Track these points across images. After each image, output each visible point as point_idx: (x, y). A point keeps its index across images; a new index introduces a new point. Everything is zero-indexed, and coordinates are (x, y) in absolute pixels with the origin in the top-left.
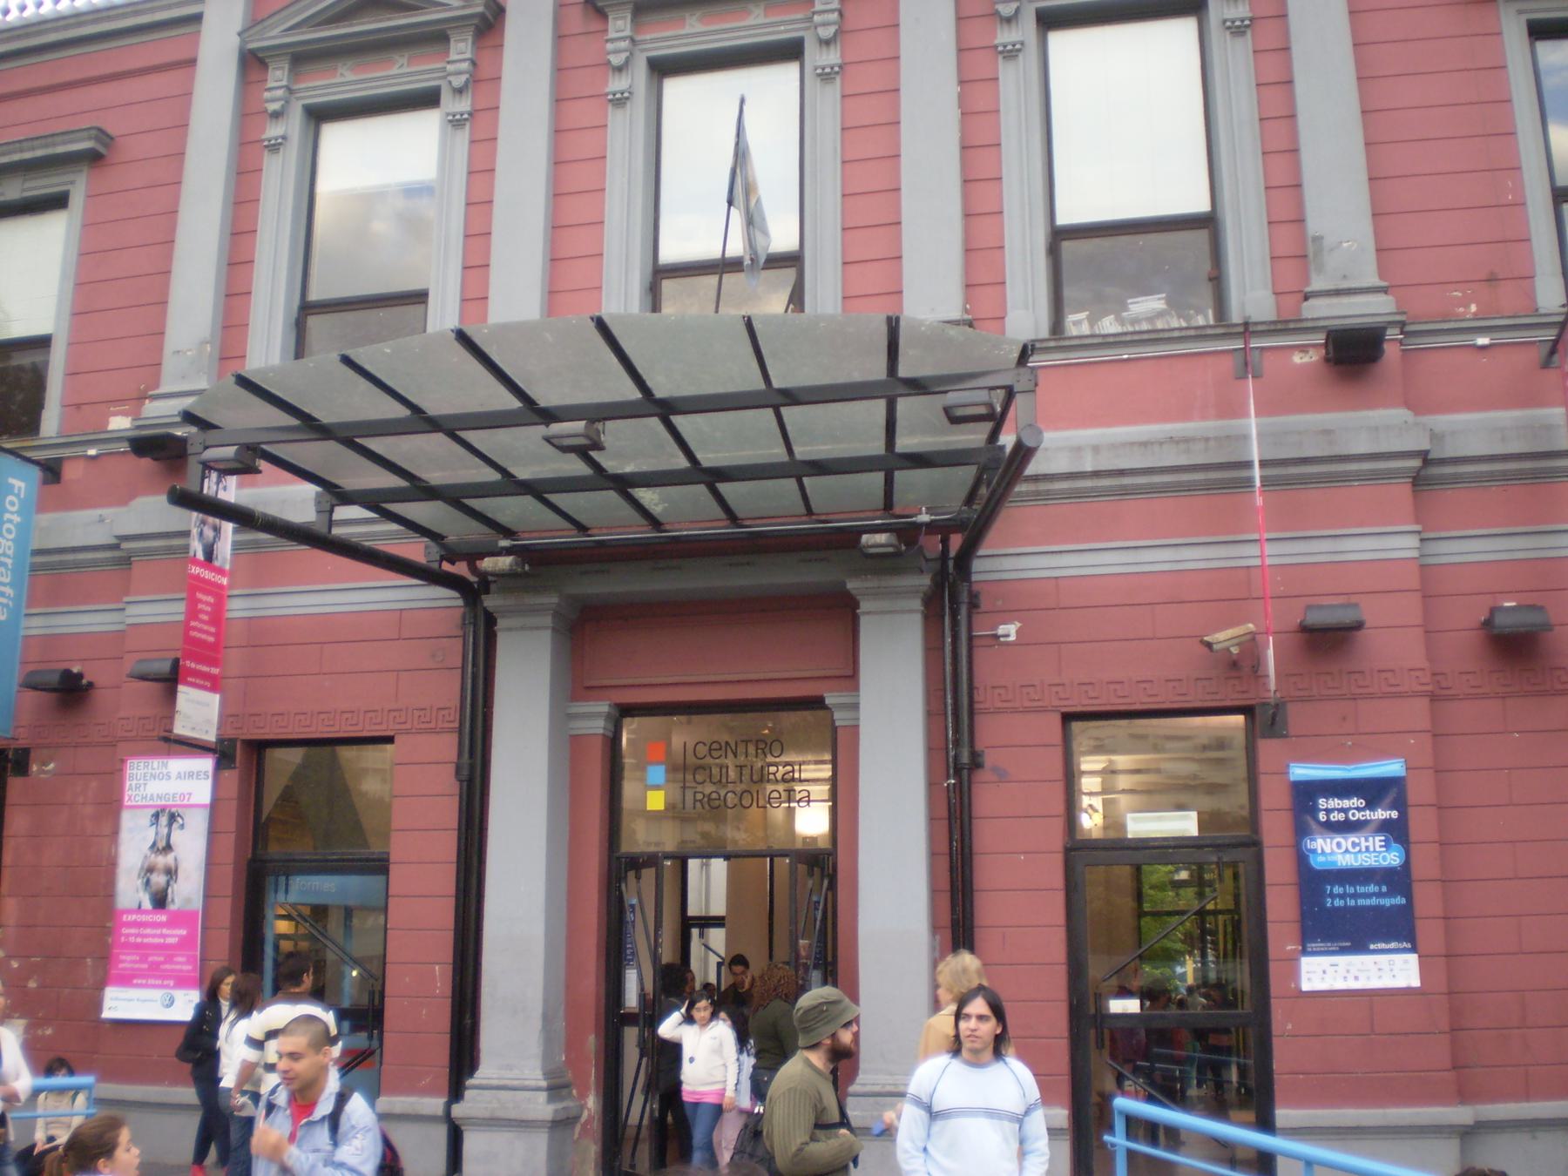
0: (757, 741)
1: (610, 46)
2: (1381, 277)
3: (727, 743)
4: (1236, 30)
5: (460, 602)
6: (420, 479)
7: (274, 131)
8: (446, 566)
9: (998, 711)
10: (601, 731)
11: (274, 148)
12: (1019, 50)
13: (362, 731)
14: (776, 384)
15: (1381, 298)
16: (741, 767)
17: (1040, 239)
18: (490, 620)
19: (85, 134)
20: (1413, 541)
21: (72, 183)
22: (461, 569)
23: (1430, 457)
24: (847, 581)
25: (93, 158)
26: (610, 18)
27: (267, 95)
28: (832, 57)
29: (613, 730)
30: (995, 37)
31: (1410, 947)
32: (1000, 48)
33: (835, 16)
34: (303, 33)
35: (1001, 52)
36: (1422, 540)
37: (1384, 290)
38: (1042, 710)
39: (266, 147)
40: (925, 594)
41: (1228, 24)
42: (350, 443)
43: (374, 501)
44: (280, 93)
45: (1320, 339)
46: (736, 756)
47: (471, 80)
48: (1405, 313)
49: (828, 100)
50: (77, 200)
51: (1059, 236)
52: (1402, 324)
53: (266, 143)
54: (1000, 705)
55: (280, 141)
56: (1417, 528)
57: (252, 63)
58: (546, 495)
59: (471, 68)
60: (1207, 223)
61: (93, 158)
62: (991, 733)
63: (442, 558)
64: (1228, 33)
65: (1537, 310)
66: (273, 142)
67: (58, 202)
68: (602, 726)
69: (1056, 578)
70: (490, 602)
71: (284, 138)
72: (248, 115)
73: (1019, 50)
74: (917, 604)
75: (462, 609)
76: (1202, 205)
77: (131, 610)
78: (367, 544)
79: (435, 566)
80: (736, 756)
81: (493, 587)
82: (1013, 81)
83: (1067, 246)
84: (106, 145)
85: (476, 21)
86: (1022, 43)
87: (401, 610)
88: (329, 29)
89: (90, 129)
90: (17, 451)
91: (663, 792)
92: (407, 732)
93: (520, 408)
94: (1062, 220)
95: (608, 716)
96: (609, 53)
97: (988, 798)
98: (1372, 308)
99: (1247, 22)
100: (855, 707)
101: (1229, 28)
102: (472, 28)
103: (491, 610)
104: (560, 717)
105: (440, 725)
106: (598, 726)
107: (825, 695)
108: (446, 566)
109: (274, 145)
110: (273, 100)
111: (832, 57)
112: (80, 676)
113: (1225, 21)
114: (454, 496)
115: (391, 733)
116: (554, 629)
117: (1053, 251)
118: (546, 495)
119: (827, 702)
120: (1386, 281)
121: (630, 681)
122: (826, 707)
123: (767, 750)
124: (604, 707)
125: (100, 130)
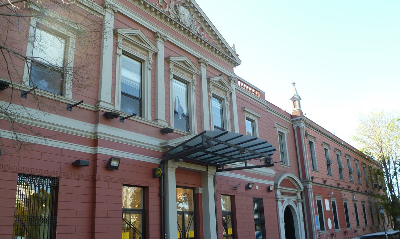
91: (329, 210)
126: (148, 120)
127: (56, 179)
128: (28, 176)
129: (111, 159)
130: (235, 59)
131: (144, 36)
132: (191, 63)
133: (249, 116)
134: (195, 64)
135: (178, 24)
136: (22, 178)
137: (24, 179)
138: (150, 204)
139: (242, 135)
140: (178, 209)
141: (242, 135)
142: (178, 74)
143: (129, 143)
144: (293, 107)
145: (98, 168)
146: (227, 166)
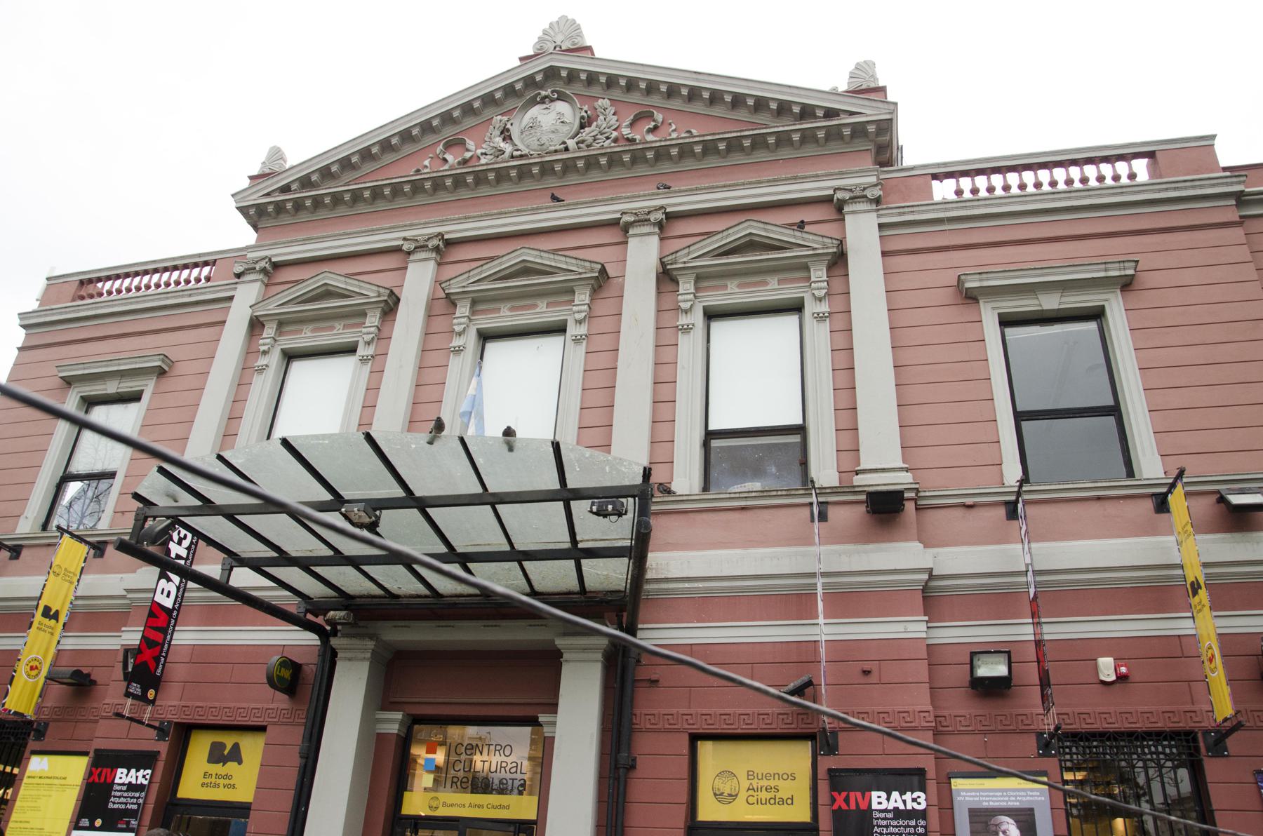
0: (496, 745)
1: (455, 321)
2: (904, 462)
3: (477, 745)
4: (820, 318)
5: (319, 643)
6: (285, 553)
7: (262, 361)
8: (309, 617)
9: (648, 731)
10: (396, 732)
11: (261, 371)
12: (691, 329)
13: (234, 721)
14: (490, 490)
15: (904, 474)
16: (484, 761)
17: (698, 436)
18: (334, 654)
19: (158, 357)
20: (923, 627)
21: (147, 385)
22: (320, 620)
23: (934, 574)
24: (555, 639)
25: (161, 372)
26: (458, 306)
27: (261, 342)
28: (583, 330)
29: (406, 732)
30: (678, 321)
31: (477, 758)
32: (680, 327)
33: (586, 307)
34: (289, 308)
35: (681, 330)
36: (928, 628)
37: (907, 470)
38: (677, 731)
39: (256, 370)
40: (605, 650)
41: (816, 315)
42: (231, 517)
43: (257, 565)
44: (268, 341)
45: (863, 497)
46: (481, 754)
47: (376, 338)
48: (918, 483)
49: (578, 354)
50: (146, 397)
51: (710, 435)
52: (917, 490)
53: (256, 368)
54: (649, 726)
55: (264, 367)
56: (926, 618)
57: (256, 325)
58: (361, 567)
59: (377, 331)
60: (801, 430)
61: (161, 372)
62: (644, 745)
63: (307, 611)
64: (815, 320)
65: (1003, 484)
66: (260, 368)
67: (135, 397)
68: (397, 728)
69: (691, 644)
70: (334, 642)
71: (267, 366)
72: (250, 351)
73: (691, 329)
74: (599, 656)
75: (319, 647)
76: (800, 422)
77: (125, 635)
78: (273, 603)
79: (302, 615)
80: (481, 754)
81: (339, 634)
82: (688, 348)
83: (715, 443)
84: (170, 367)
85: (382, 305)
86: (693, 325)
87: (284, 645)
88: (304, 306)
89: (159, 355)
90: (82, 537)
92: (275, 724)
93: (332, 500)
94: (711, 428)
95: (402, 723)
96: (455, 325)
97: (639, 789)
98: (902, 480)
99: (826, 314)
100: (554, 724)
101: (815, 318)
102: (380, 309)
103: (334, 646)
104: (368, 720)
105: (296, 720)
106: (394, 728)
107: (539, 715)
108: (309, 617)
109: (260, 370)
110: (264, 345)
111: (583, 330)
112: (88, 675)
113: (813, 314)
114: (306, 564)
115: (265, 724)
116: (371, 662)
117: (706, 445)
118: (361, 567)
119: (540, 719)
120: (906, 464)
121: (417, 700)
122: (540, 725)
123: (502, 752)
124: (399, 716)
125: (165, 356)
126: (1006, 484)
127: (1183, 737)
128: (1114, 737)
129: (976, 653)
130: (852, 113)
131: (339, 278)
132: (552, 256)
133: (1036, 302)
134: (560, 253)
135: (602, 154)
136: (1164, 747)
137: (1149, 747)
138: (1208, 779)
139: (268, 438)
140: (840, 799)
141: (268, 438)
142: (507, 316)
143: (1089, 580)
144: (233, 192)
145: (1037, 681)
146: (477, 592)
